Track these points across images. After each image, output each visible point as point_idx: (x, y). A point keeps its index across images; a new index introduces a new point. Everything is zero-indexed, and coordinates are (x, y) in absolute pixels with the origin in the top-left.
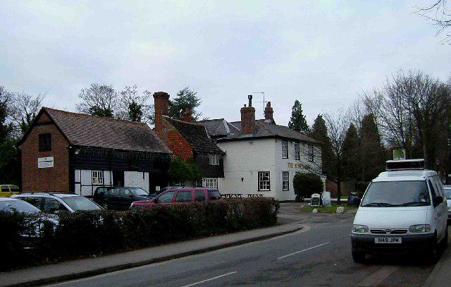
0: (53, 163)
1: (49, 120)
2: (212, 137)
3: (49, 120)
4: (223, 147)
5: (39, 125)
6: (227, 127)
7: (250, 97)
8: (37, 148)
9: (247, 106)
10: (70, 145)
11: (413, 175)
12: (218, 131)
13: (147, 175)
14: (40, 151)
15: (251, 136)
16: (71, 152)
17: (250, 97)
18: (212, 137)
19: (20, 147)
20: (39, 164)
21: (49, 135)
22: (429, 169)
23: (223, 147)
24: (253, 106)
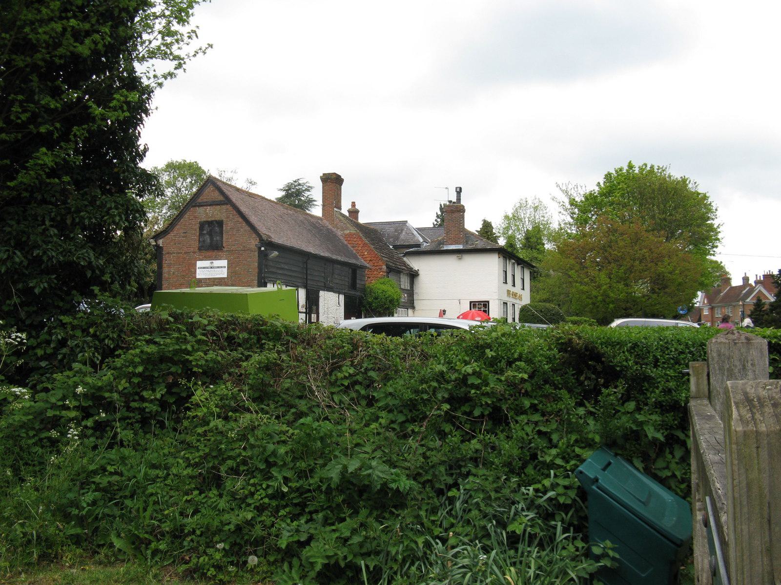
0: (225, 270)
1: (221, 198)
2: (395, 247)
3: (221, 198)
4: (415, 263)
5: (201, 205)
6: (415, 233)
7: (459, 191)
8: (196, 244)
9: (454, 200)
10: (261, 239)
11: (227, 290)
12: (403, 239)
13: (342, 297)
14: (200, 249)
15: (461, 247)
16: (263, 256)
17: (459, 191)
18: (395, 247)
19: (160, 242)
20: (198, 271)
21: (220, 223)
22: (753, 322)
23: (415, 263)
24: (462, 203)
